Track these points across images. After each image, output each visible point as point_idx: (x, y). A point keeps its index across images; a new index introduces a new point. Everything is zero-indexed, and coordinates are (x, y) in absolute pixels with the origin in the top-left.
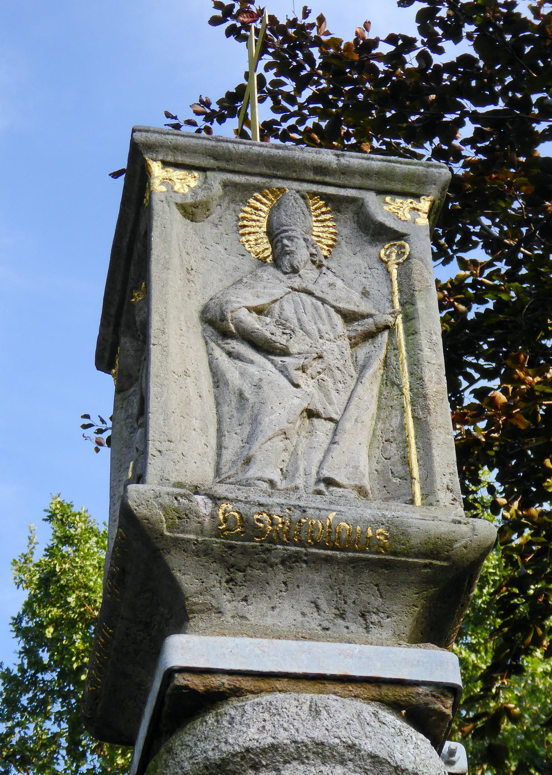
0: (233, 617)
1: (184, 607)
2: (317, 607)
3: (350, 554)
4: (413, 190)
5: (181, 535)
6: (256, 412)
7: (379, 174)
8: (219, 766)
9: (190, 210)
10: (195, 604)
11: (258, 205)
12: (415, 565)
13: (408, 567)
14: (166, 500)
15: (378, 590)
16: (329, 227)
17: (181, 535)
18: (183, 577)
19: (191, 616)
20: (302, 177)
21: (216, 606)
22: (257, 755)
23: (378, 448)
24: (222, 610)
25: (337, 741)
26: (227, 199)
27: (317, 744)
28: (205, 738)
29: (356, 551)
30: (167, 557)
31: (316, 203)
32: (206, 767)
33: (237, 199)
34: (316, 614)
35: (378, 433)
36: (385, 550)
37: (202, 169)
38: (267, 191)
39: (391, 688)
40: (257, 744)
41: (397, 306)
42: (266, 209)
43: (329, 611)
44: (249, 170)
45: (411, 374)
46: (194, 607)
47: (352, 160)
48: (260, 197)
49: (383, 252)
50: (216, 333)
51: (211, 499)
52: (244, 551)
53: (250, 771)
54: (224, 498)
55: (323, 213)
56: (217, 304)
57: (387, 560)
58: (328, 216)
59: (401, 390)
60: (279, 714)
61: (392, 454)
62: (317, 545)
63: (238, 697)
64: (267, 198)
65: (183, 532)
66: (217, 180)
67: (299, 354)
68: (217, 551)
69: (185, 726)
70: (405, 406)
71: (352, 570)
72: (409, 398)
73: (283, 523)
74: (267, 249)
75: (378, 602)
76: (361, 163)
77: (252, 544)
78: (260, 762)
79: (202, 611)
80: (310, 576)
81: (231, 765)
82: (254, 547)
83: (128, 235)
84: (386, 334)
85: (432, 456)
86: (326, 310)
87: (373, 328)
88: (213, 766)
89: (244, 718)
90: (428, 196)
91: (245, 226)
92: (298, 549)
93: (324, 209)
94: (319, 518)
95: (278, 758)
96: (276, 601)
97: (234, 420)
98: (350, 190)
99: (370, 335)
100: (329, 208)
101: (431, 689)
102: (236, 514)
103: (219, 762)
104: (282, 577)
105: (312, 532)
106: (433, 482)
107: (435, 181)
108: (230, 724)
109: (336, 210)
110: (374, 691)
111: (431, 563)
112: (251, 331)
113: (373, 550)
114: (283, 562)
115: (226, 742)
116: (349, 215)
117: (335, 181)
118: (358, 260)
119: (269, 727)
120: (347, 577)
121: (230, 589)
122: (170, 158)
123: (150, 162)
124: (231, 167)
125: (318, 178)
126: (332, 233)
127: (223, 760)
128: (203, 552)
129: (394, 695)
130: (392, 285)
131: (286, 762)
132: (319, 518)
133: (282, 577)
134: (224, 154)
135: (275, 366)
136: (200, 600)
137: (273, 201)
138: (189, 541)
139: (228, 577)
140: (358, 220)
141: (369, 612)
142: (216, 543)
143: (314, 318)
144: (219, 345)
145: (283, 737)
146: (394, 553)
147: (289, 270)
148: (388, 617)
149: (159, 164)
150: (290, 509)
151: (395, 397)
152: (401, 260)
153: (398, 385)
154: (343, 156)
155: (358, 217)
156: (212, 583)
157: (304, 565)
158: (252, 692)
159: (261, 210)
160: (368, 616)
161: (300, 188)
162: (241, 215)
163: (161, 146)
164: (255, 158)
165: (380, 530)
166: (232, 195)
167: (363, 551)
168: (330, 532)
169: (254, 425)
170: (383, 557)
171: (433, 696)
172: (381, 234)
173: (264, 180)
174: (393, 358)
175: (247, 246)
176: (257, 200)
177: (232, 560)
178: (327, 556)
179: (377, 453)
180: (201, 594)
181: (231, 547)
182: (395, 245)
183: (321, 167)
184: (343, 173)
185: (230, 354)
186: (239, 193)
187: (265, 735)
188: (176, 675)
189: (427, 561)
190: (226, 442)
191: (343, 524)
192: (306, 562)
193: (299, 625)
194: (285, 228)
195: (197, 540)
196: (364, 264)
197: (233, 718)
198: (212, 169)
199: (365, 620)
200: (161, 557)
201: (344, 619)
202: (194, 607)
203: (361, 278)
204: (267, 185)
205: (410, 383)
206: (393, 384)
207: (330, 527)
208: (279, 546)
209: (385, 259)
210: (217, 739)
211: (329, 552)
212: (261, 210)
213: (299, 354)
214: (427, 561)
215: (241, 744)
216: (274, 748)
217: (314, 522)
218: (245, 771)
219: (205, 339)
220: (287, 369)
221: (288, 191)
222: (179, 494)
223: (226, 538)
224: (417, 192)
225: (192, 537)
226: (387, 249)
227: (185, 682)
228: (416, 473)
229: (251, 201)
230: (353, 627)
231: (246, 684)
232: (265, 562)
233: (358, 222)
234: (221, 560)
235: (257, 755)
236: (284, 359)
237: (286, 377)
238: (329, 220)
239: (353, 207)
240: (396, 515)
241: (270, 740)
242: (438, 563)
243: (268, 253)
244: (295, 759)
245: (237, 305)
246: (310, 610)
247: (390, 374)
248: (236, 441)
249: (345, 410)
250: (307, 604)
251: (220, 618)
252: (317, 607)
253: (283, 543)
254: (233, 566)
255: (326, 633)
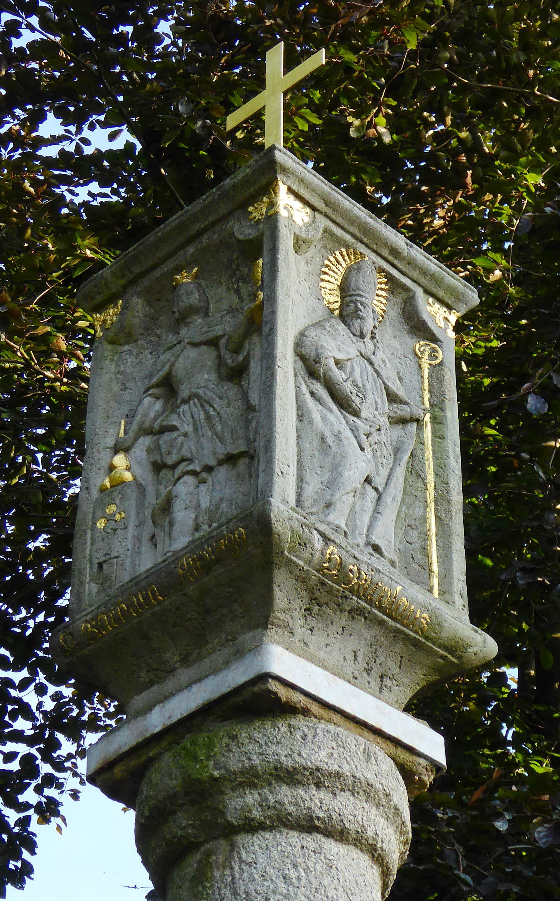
0: (299, 641)
1: (267, 617)
2: (355, 656)
3: (398, 625)
4: (450, 302)
5: (295, 559)
6: (337, 462)
7: (433, 277)
8: (288, 772)
9: (300, 242)
10: (277, 618)
11: (340, 259)
12: (436, 653)
13: (430, 652)
14: (296, 525)
15: (401, 661)
16: (382, 303)
17: (295, 559)
18: (279, 592)
19: (270, 626)
20: (379, 252)
21: (291, 627)
22: (323, 776)
23: (401, 529)
24: (294, 632)
25: (381, 787)
26: (322, 243)
27: (368, 785)
28: (278, 743)
29: (402, 624)
30: (276, 572)
31: (380, 278)
32: (276, 769)
33: (328, 247)
34: (352, 662)
35: (402, 515)
36: (422, 633)
37: (314, 209)
38: (352, 251)
39: (404, 751)
40: (327, 767)
41: (428, 406)
42: (344, 265)
43: (362, 664)
44: (346, 226)
45: (436, 475)
46: (275, 620)
47: (418, 255)
48: (345, 253)
49: (418, 346)
50: (304, 370)
51: (321, 536)
52: (330, 591)
53: (313, 786)
54: (333, 541)
55: (382, 289)
56: (313, 345)
57: (420, 641)
58: (384, 293)
59: (425, 484)
60: (344, 748)
61: (414, 541)
62: (380, 608)
63: (305, 716)
64: (349, 257)
65: (297, 556)
66: (323, 222)
67: (366, 420)
68: (312, 583)
69: (252, 721)
70: (429, 501)
71: (392, 638)
72: (432, 497)
73: (366, 581)
74: (337, 302)
75: (395, 670)
76: (423, 261)
77: (338, 587)
78: (324, 782)
79: (279, 626)
80: (363, 630)
81: (300, 775)
82: (338, 591)
83: (207, 223)
84: (415, 425)
85: (451, 559)
86: (380, 383)
87: (408, 417)
88: (284, 770)
89: (316, 740)
90: (458, 312)
91: (326, 273)
92: (366, 605)
93: (383, 286)
94: (390, 587)
95: (338, 784)
96: (331, 640)
97: (315, 460)
98: (407, 279)
99: (403, 421)
100: (387, 287)
101: (428, 763)
102: (338, 558)
103: (290, 769)
104: (343, 623)
105: (382, 597)
106: (451, 583)
107: (468, 302)
108: (304, 740)
109: (391, 291)
110: (392, 749)
111: (446, 656)
112: (335, 382)
113: (414, 629)
114: (350, 612)
115: (299, 754)
116: (399, 300)
117: (401, 267)
118: (395, 343)
119: (336, 755)
120: (386, 642)
121: (305, 616)
122: (295, 188)
123: (280, 183)
124: (334, 217)
125: (390, 258)
126: (382, 310)
127: (295, 769)
128: (302, 579)
129: (404, 758)
130: (423, 382)
131: (342, 790)
132: (390, 587)
133: (343, 623)
134: (334, 203)
135: (347, 422)
136: (282, 616)
137: (351, 261)
138: (298, 565)
139: (308, 606)
140: (404, 308)
141: (387, 676)
142: (315, 576)
143: (372, 387)
144: (305, 382)
145: (346, 769)
146: (427, 638)
147: (358, 334)
148: (397, 685)
149: (286, 187)
150: (372, 570)
151: (420, 489)
152: (433, 362)
153: (422, 479)
154: (412, 247)
155: (405, 305)
156: (295, 607)
157: (363, 620)
158: (316, 717)
159: (341, 265)
160: (384, 679)
161: (375, 261)
162: (326, 262)
163: (293, 174)
164: (355, 218)
165: (425, 615)
166: (326, 242)
167: (407, 626)
168: (393, 602)
169: (335, 473)
170: (418, 637)
171: (426, 769)
172: (419, 329)
173: (353, 240)
174: (419, 451)
175: (323, 292)
176: (341, 254)
177: (317, 594)
178: (383, 620)
179: (401, 534)
180: (284, 612)
181: (323, 584)
182: (429, 345)
183: (397, 249)
184: (409, 263)
185: (312, 394)
186: (332, 242)
187: (333, 762)
188: (270, 680)
189: (445, 654)
190: (308, 476)
191: (404, 599)
192: (365, 618)
193: (340, 667)
194: (361, 293)
195: (303, 568)
196: (400, 351)
197: (306, 735)
198: (320, 212)
199: (382, 681)
200: (271, 570)
201: (368, 674)
202: (275, 620)
203: (396, 361)
204: (355, 246)
205: (435, 482)
206: (418, 476)
207: (395, 598)
208: (355, 598)
209: (419, 353)
210: (291, 748)
211: (385, 618)
212: (341, 265)
213: (366, 420)
214: (445, 654)
215: (313, 761)
216: (338, 775)
217: (386, 589)
218: (309, 785)
219: (295, 371)
220: (358, 431)
221: (366, 259)
222: (304, 523)
223: (323, 574)
224: (452, 305)
225: (301, 563)
226: (422, 346)
227: (276, 690)
228: (435, 567)
229: (337, 253)
230: (373, 684)
231: (315, 708)
232: (339, 606)
233: (404, 310)
234: (311, 591)
235: (323, 776)
236: (355, 419)
237: (356, 437)
238: (383, 297)
239: (404, 295)
240: (438, 607)
241: (336, 768)
242: (451, 658)
243: (337, 306)
244: (349, 790)
245: (330, 354)
246: (350, 657)
247: (415, 464)
248: (316, 481)
249: (386, 484)
250: (351, 651)
251: (290, 637)
252: (355, 656)
253: (358, 597)
254: (315, 599)
255: (353, 680)
